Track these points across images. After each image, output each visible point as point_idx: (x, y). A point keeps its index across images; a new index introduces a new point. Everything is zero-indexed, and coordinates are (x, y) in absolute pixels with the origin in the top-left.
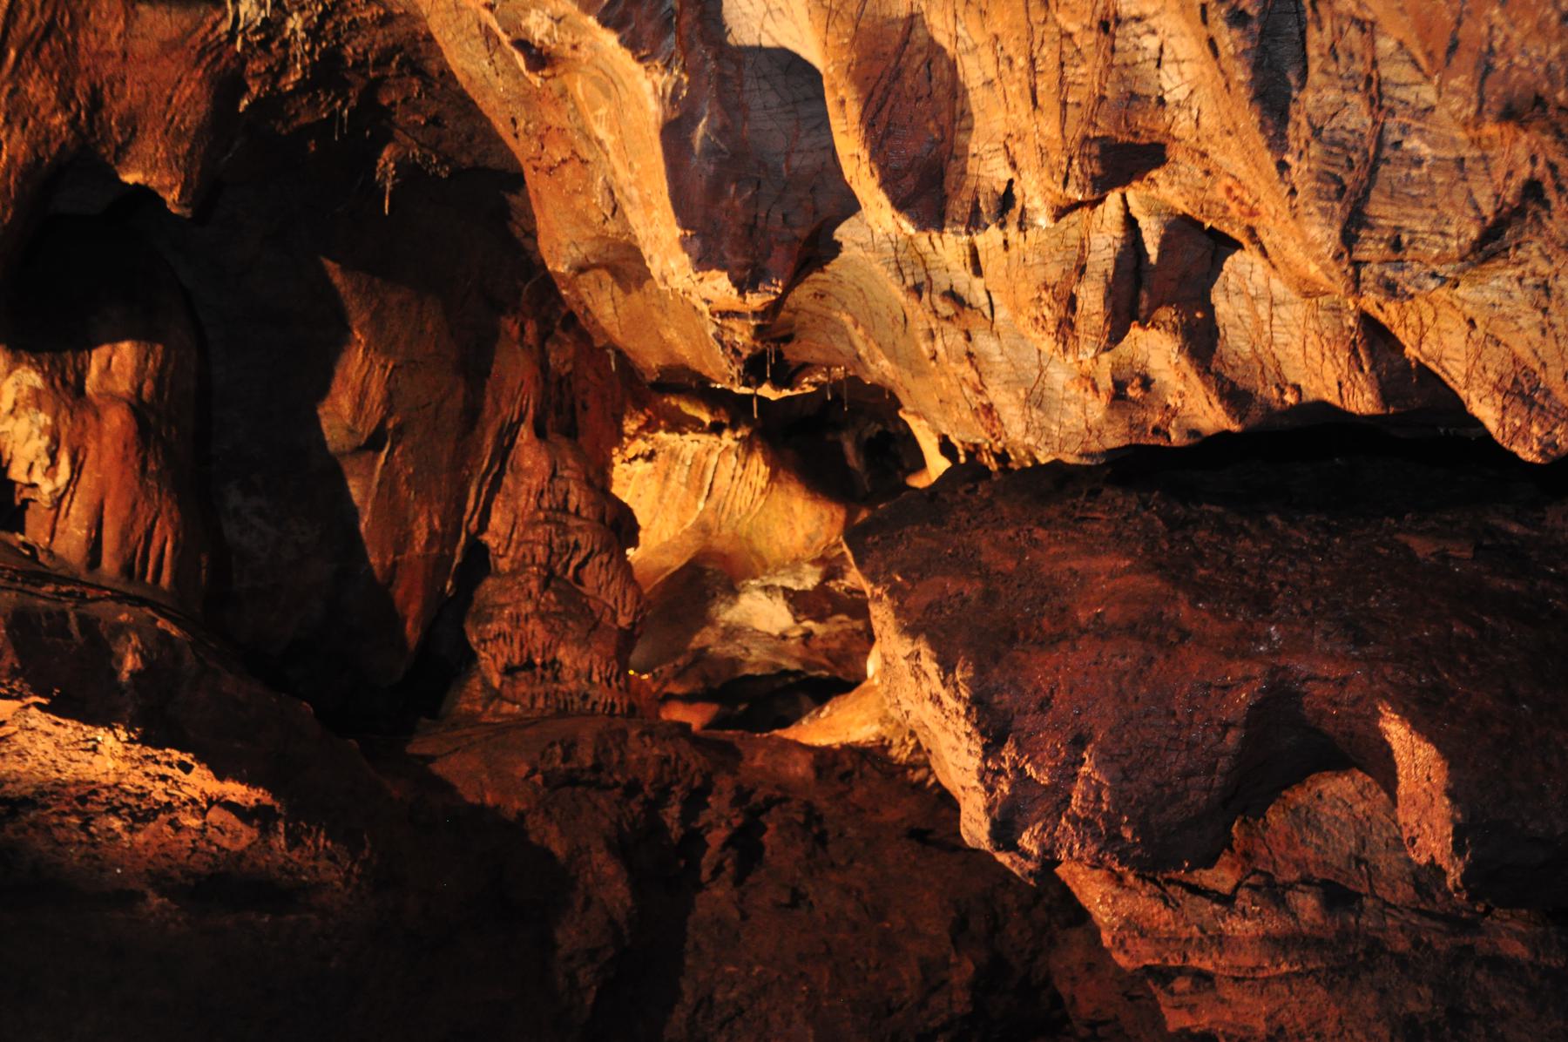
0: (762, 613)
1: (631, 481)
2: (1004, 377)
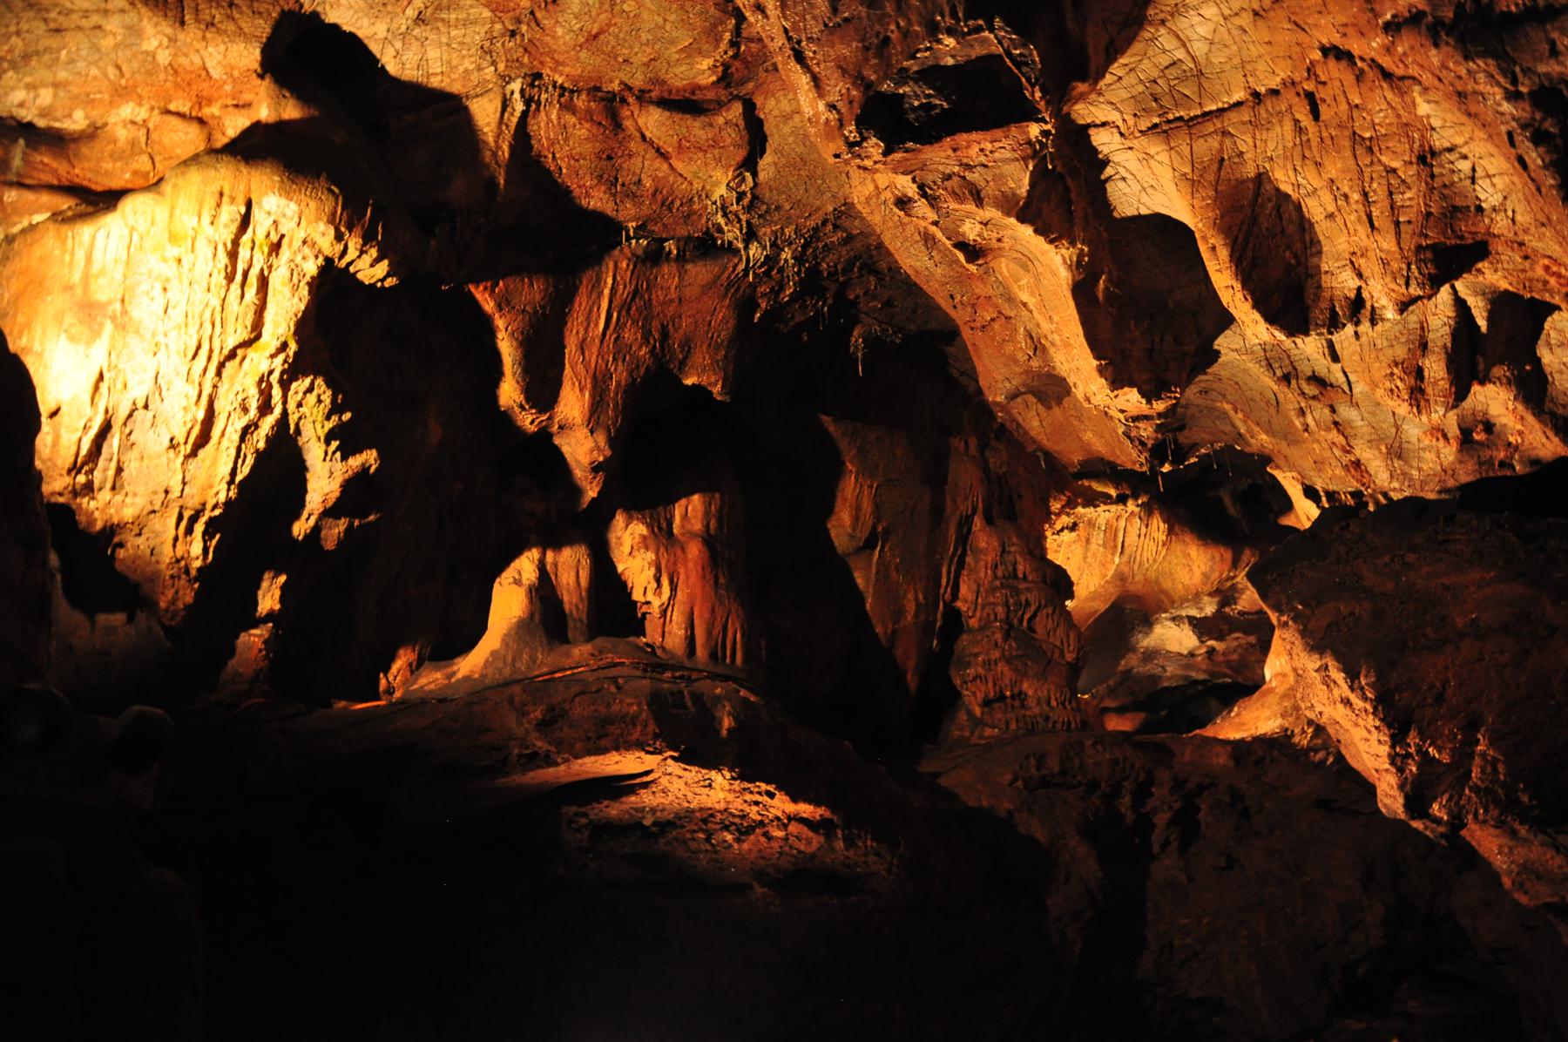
0: (1173, 637)
1: (1062, 548)
2: (1367, 437)
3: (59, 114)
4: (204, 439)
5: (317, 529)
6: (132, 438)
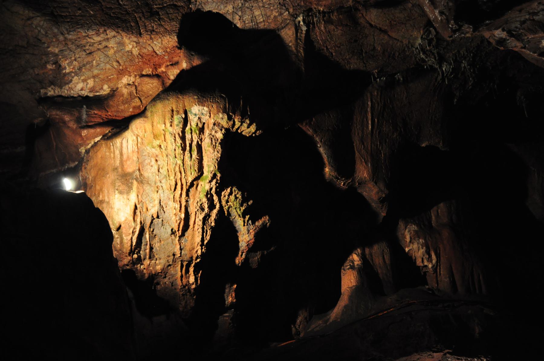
3: (97, 89)
4: (186, 227)
5: (247, 259)
6: (154, 233)
